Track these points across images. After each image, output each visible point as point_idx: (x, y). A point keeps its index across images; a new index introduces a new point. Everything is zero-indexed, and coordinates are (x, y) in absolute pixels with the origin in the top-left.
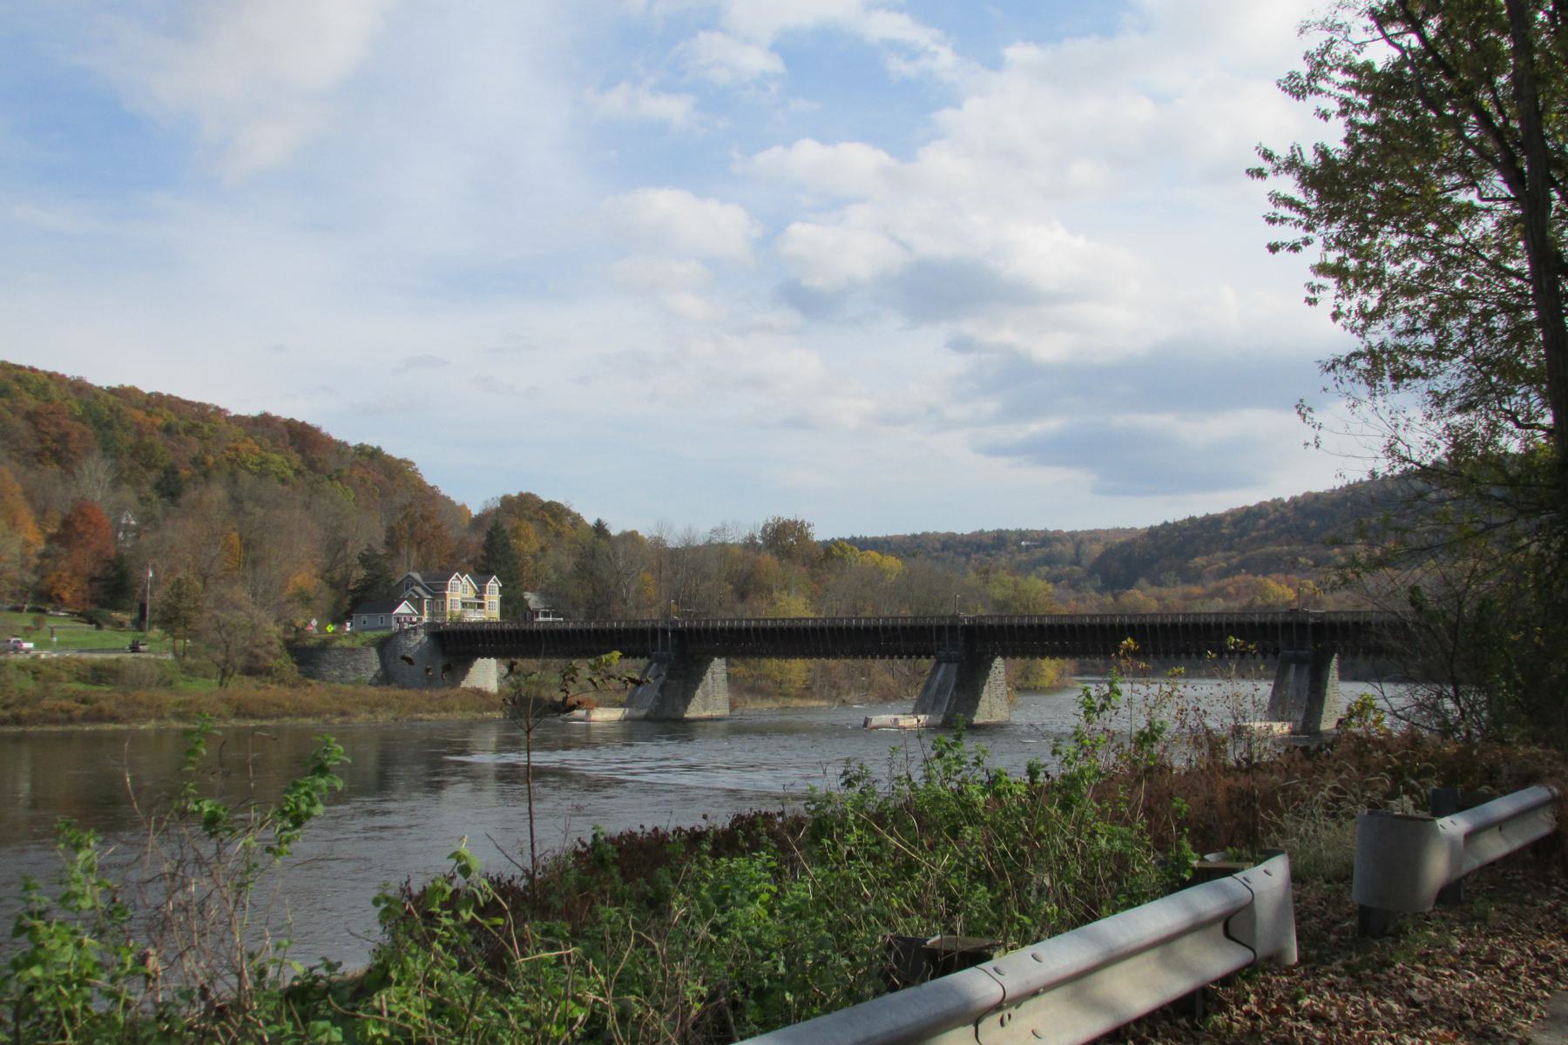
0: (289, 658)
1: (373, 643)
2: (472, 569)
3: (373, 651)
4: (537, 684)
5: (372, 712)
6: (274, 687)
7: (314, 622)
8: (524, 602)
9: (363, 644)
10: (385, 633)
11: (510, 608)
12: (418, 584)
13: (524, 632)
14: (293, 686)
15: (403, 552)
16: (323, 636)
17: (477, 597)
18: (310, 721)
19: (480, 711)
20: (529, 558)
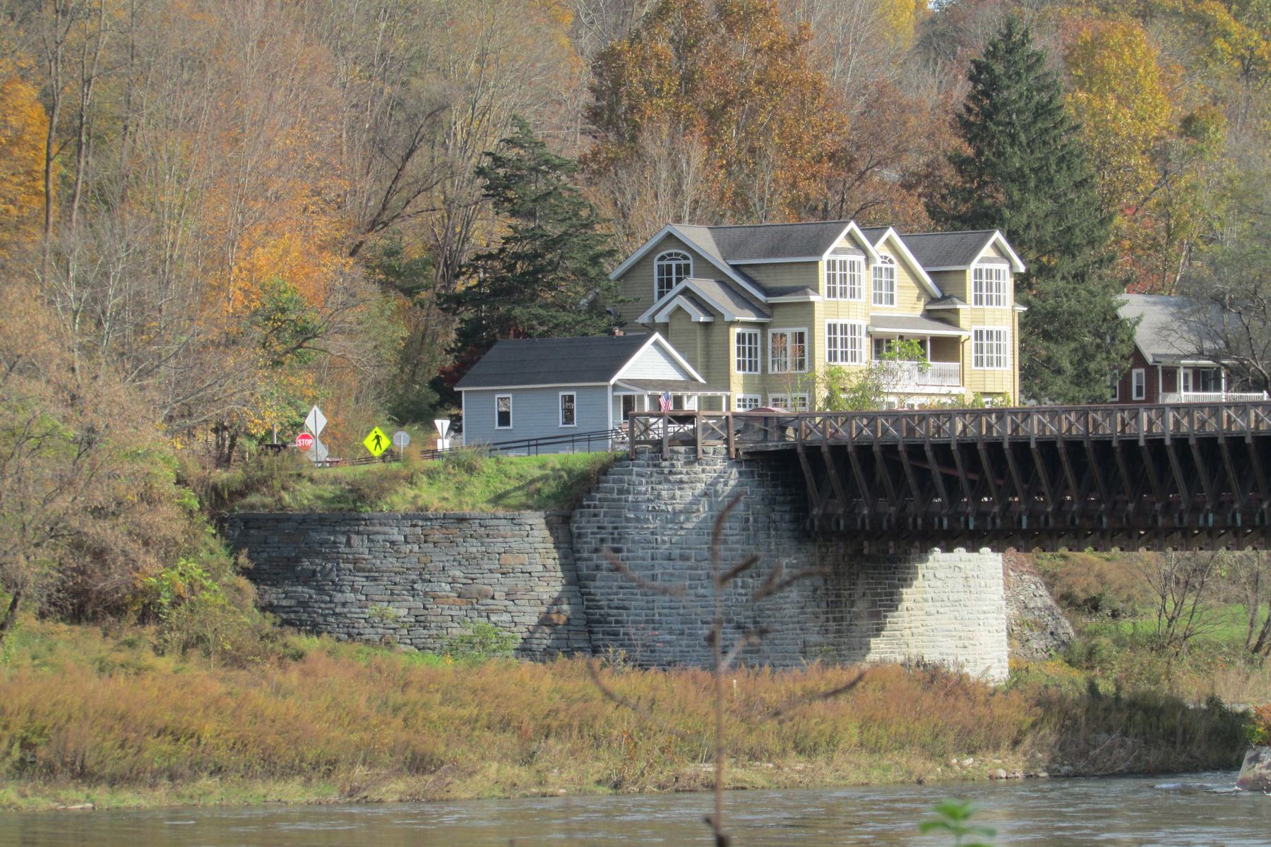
0: (222, 556)
1: (534, 497)
2: (918, 207)
3: (536, 520)
4: (1158, 644)
5: (528, 759)
6: (167, 663)
7: (316, 421)
8: (1112, 326)
9: (498, 499)
10: (578, 458)
11: (1063, 354)
12: (708, 270)
13: (1103, 446)
14: (235, 660)
15: (653, 146)
16: (347, 472)
17: (929, 315)
18: (293, 792)
19: (933, 752)
20: (1137, 160)
